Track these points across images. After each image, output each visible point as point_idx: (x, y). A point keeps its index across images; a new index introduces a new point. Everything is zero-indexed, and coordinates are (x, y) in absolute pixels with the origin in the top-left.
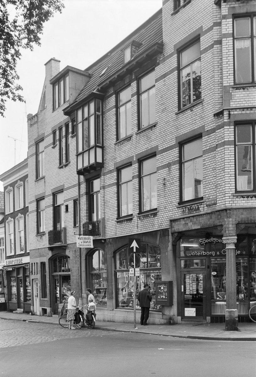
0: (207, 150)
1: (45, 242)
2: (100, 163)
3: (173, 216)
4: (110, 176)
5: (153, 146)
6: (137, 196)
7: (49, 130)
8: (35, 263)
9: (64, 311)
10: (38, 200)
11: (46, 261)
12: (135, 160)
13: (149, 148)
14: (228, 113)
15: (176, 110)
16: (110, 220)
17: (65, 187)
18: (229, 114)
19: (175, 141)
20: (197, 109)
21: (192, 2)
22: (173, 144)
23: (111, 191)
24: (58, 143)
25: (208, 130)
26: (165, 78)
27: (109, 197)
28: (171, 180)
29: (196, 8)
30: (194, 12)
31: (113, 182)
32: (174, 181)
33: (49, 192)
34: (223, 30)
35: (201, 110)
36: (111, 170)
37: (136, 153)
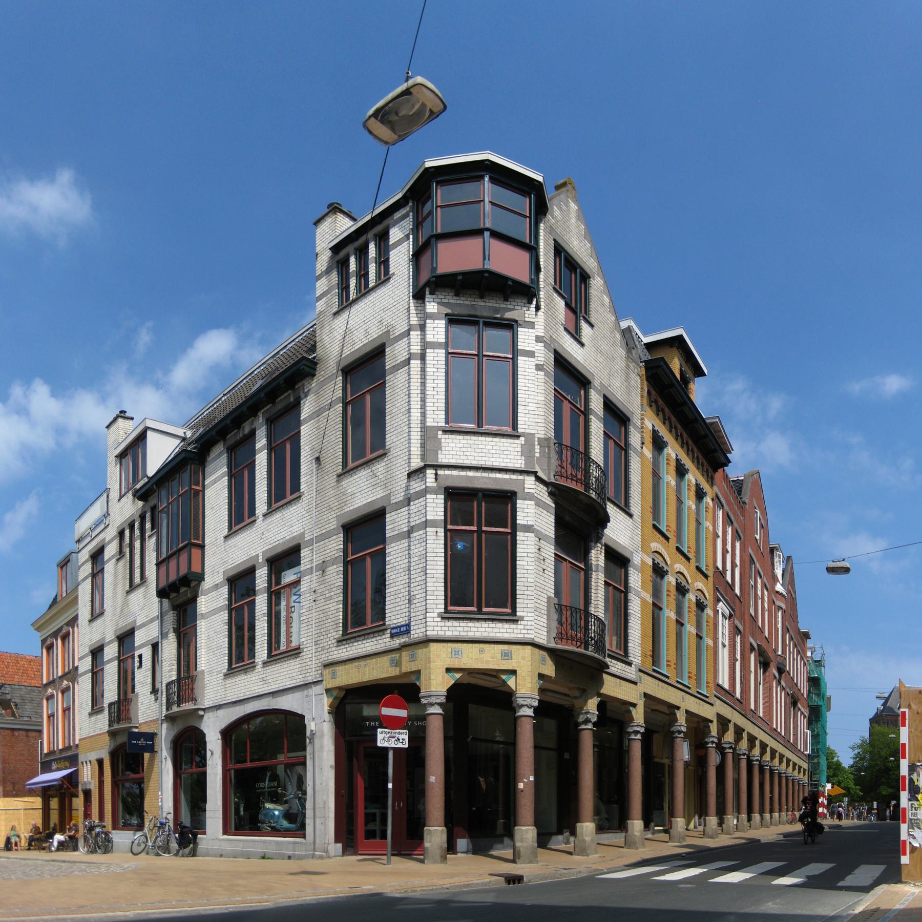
1: (102, 722)
2: (200, 573)
5: (295, 534)
6: (112, 426)
8: (86, 762)
9: (703, 823)
10: (97, 652)
11: (103, 757)
12: (260, 561)
13: (288, 538)
15: (339, 469)
16: (215, 674)
17: (138, 625)
18: (436, 474)
20: (379, 467)
22: (333, 527)
24: (127, 551)
25: (396, 503)
26: (320, 417)
27: (213, 632)
28: (327, 592)
29: (379, 303)
30: (375, 309)
31: (221, 605)
33: (110, 635)
34: (427, 336)
35: (385, 467)
36: (217, 584)
37: (264, 549)
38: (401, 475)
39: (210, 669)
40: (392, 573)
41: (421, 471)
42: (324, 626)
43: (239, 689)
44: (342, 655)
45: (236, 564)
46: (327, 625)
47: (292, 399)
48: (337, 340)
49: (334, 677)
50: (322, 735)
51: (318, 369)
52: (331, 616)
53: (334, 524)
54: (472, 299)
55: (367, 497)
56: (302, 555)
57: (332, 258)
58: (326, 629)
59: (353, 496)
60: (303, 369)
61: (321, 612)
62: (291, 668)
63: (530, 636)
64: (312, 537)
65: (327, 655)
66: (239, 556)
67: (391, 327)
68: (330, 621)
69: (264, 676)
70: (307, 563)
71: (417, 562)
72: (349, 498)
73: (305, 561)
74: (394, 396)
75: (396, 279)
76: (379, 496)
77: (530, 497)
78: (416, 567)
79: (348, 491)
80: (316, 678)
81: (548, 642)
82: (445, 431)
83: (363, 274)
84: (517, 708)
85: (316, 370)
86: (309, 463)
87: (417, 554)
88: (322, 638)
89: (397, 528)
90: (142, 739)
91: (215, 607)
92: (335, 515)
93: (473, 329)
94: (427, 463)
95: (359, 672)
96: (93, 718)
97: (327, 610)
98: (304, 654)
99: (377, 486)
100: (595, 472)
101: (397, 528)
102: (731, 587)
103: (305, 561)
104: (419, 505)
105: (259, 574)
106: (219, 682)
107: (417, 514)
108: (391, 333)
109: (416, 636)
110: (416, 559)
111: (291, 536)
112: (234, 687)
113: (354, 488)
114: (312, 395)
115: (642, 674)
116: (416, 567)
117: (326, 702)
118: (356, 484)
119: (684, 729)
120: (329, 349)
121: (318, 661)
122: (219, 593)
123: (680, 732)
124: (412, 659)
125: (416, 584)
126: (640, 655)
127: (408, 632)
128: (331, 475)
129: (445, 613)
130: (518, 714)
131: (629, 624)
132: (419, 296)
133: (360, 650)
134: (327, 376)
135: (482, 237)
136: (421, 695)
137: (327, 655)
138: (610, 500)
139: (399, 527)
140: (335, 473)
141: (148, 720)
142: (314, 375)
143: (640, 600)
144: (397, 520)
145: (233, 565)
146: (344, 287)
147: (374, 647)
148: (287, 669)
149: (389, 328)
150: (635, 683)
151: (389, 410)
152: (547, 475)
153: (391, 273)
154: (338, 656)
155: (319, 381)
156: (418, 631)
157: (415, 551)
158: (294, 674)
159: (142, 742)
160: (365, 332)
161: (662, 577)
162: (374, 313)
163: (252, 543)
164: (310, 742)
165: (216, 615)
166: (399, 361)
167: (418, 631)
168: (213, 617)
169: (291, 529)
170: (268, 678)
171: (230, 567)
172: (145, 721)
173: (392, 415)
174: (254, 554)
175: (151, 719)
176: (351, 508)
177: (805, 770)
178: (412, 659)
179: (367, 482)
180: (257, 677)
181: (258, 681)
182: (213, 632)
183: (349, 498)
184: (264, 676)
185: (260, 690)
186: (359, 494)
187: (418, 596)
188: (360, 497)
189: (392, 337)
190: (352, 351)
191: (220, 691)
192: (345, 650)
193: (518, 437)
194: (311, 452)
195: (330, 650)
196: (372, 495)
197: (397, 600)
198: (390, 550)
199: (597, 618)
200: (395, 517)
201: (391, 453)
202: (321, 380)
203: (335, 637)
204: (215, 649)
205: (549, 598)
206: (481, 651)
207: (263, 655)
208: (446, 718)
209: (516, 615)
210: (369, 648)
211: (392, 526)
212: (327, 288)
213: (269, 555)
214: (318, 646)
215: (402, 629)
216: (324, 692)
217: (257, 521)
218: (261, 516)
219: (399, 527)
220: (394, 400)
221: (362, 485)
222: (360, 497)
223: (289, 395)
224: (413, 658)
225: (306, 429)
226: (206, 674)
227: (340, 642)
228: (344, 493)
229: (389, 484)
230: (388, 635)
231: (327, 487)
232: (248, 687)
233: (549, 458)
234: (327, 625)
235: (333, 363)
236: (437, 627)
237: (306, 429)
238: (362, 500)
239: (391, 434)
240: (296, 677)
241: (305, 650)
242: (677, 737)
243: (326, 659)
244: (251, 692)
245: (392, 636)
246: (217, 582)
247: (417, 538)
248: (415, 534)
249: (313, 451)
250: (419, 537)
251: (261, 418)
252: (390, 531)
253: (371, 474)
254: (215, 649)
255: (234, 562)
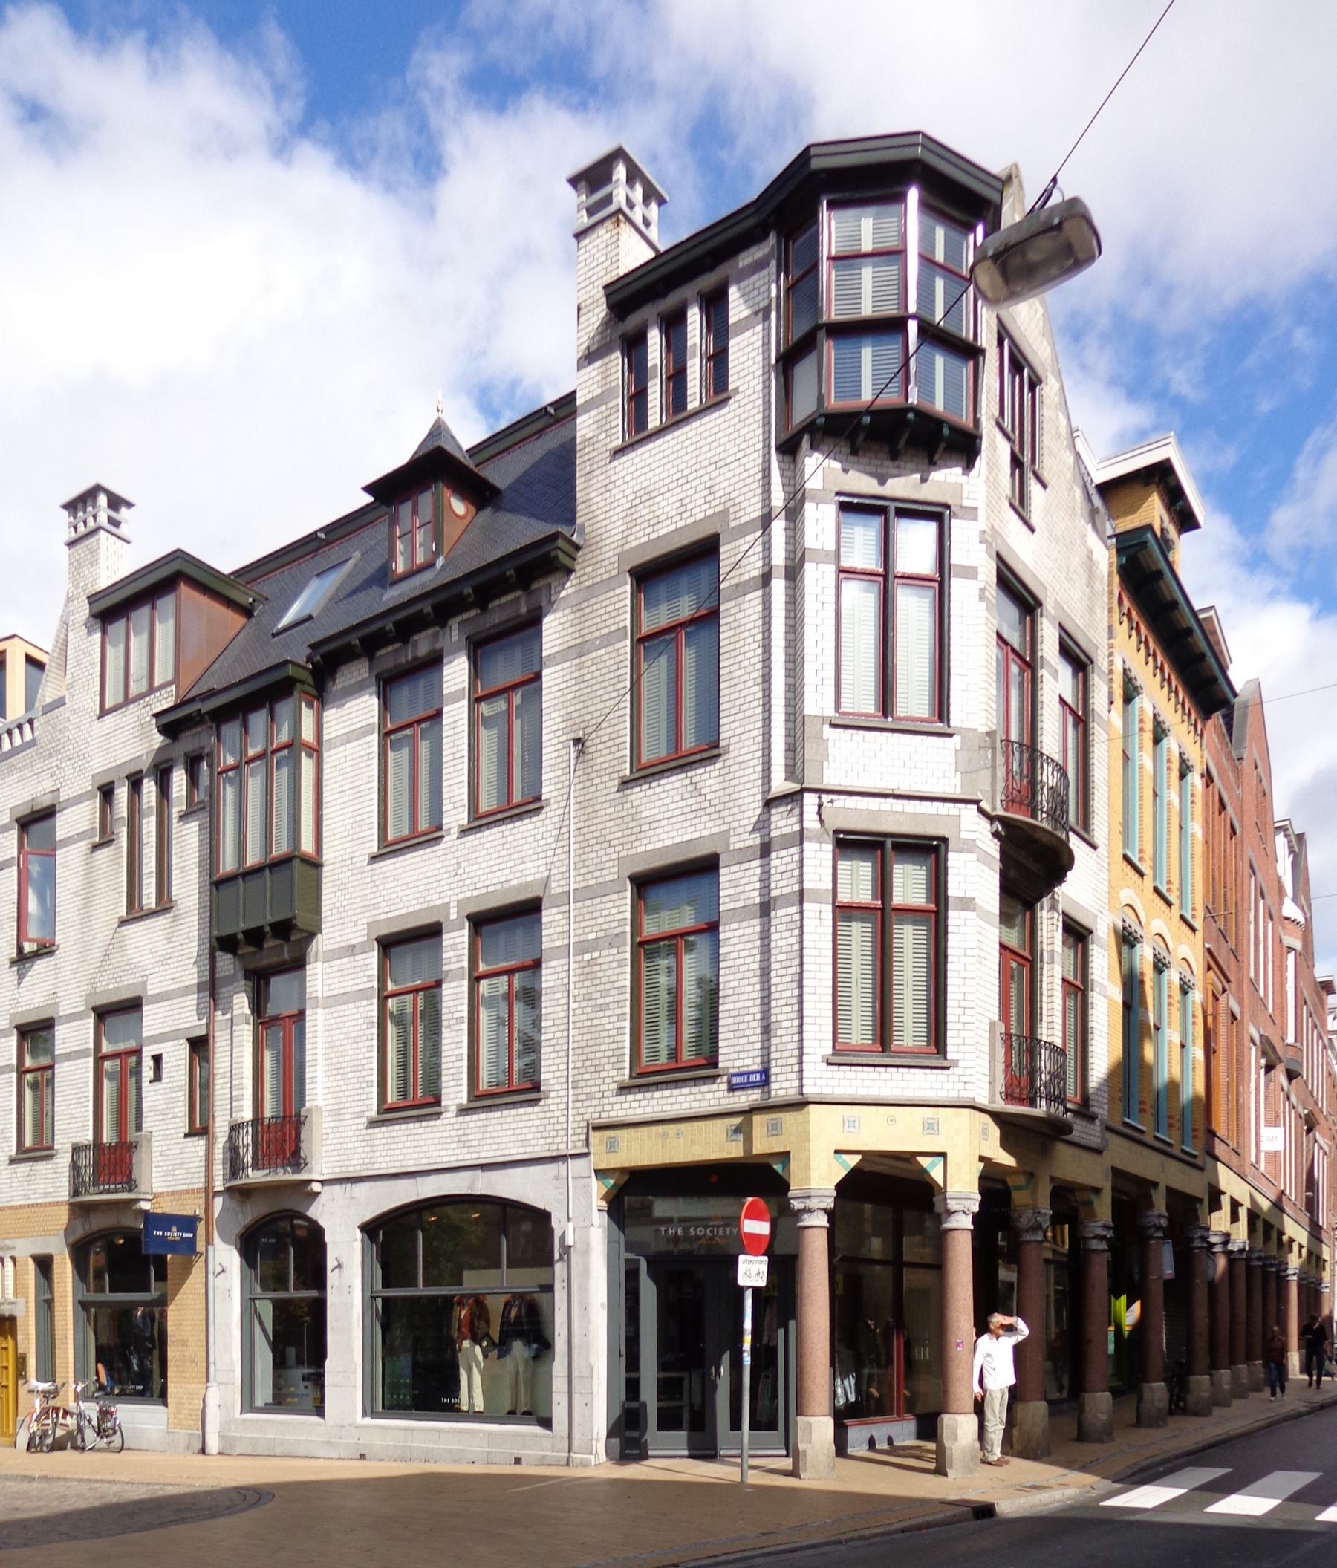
0: (738, 911)
3: (604, 1115)
4: (349, 966)
5: (530, 878)
7: (79, 782)
12: (453, 916)
13: (514, 883)
14: (816, 801)
19: (615, 869)
20: (707, 776)
21: (4, 1472)
23: (351, 1018)
25: (740, 849)
26: (583, 659)
27: (342, 1037)
28: (598, 995)
32: (609, 999)
36: (354, 946)
38: (750, 799)
39: (336, 1107)
40: (731, 977)
41: (793, 798)
42: (592, 1056)
43: (405, 1151)
44: (630, 1112)
45: (396, 913)
46: (599, 1055)
47: (524, 610)
48: (620, 509)
49: (612, 1147)
50: (587, 1251)
51: (580, 560)
52: (607, 1040)
53: (611, 873)
54: (878, 462)
55: (681, 832)
56: (544, 920)
57: (606, 324)
58: (597, 1062)
59: (653, 826)
60: (556, 557)
61: (585, 1030)
62: (521, 1124)
63: (966, 1096)
64: (566, 889)
65: (599, 1109)
66: (405, 899)
67: (732, 503)
68: (603, 1047)
69: (461, 1132)
70: (555, 937)
71: (784, 964)
72: (644, 828)
73: (552, 931)
74: (738, 645)
75: (742, 403)
76: (706, 833)
77: (970, 847)
78: (781, 973)
79: (644, 815)
80: (575, 1147)
81: (992, 1100)
82: (833, 726)
83: (677, 378)
84: (944, 1216)
85: (575, 559)
86: (561, 746)
87: (784, 950)
88: (586, 1076)
89: (742, 896)
90: (174, 1229)
91: (348, 989)
92: (615, 856)
93: (877, 522)
94: (804, 785)
95: (663, 1146)
96: (24, 1168)
97: (599, 1028)
98: (550, 1101)
99: (702, 812)
100: (1048, 777)
101: (742, 896)
102: (1263, 1002)
103: (552, 931)
104: (789, 859)
105: (451, 942)
106: (357, 1133)
107: (785, 876)
108: (732, 517)
109: (782, 1092)
110: (783, 957)
111: (522, 880)
112: (394, 1146)
113: (656, 811)
114: (567, 612)
115: (1108, 1135)
116: (781, 973)
117: (597, 1190)
118: (660, 803)
119: (1164, 1222)
120: (604, 523)
121: (579, 1118)
122: (356, 964)
123: (1158, 1228)
124: (774, 1132)
125: (783, 1002)
126: (1106, 1101)
127: (765, 1082)
128: (607, 778)
129: (833, 1055)
130: (947, 1225)
131: (1090, 1049)
132: (789, 449)
133: (667, 1108)
134: (598, 579)
135: (900, 340)
136: (790, 1194)
137: (599, 1109)
138: (1072, 829)
139: (746, 895)
140: (616, 775)
141: (180, 1188)
142: (569, 571)
143: (1106, 1000)
144: (743, 881)
145: (390, 915)
146: (638, 398)
147: (695, 1104)
148: (514, 1125)
149: (728, 505)
150: (1098, 1151)
151: (727, 670)
152: (990, 800)
153: (731, 387)
154: (621, 1113)
155: (583, 586)
156: (785, 1085)
157: (780, 943)
158: (529, 1137)
159: (173, 1234)
160: (679, 504)
161: (1132, 946)
162: (698, 467)
163: (434, 879)
164: (561, 1259)
165: (351, 1005)
166: (746, 577)
167: (785, 1085)
168: (344, 1007)
169: (521, 867)
170: (470, 1137)
171: (384, 916)
172: (170, 1189)
173: (733, 682)
174: (439, 902)
175: (185, 1187)
176: (650, 847)
177: (1301, 1247)
178: (774, 1132)
179: (682, 804)
180: (446, 1134)
181: (449, 1140)
182: (342, 1037)
183: (644, 828)
184: (461, 1132)
185: (453, 1158)
186: (665, 822)
187: (785, 1024)
188: (667, 829)
189: (733, 524)
190: (652, 536)
191: (359, 1150)
192: (635, 1104)
193: (951, 735)
194: (564, 725)
195: (606, 1101)
196: (692, 829)
197: (742, 1026)
198: (728, 935)
199: (1051, 1047)
200: (738, 875)
201: (731, 755)
202: (587, 584)
203: (615, 1079)
204: (348, 1070)
205: (992, 1024)
206: (891, 1120)
207: (459, 1095)
208: (831, 1232)
209: (945, 1058)
210: (685, 1106)
211: (731, 891)
212: (599, 391)
213: (473, 908)
214: (579, 1091)
215: (752, 1078)
216: (593, 1174)
217: (445, 839)
218: (456, 830)
219: (746, 895)
220: (737, 652)
221: (671, 807)
222: (667, 829)
223: (518, 599)
224: (775, 1130)
225: (553, 676)
226: (325, 1114)
227: (624, 1089)
228: (635, 816)
229: (726, 813)
230: (725, 1086)
231: (600, 800)
232: (425, 1149)
233: (994, 767)
234: (599, 1055)
235: (611, 553)
236: (820, 1080)
237: (553, 676)
238: (671, 834)
239: (732, 719)
240: (533, 1142)
241: (552, 1094)
242: (1151, 1238)
243: (597, 1115)
244: (432, 1160)
245: (732, 1088)
246: (353, 942)
247: (784, 919)
248: (780, 912)
249: (570, 723)
250: (788, 919)
251: (455, 633)
252: (727, 899)
253: (690, 788)
254: (348, 1070)
255: (393, 908)
